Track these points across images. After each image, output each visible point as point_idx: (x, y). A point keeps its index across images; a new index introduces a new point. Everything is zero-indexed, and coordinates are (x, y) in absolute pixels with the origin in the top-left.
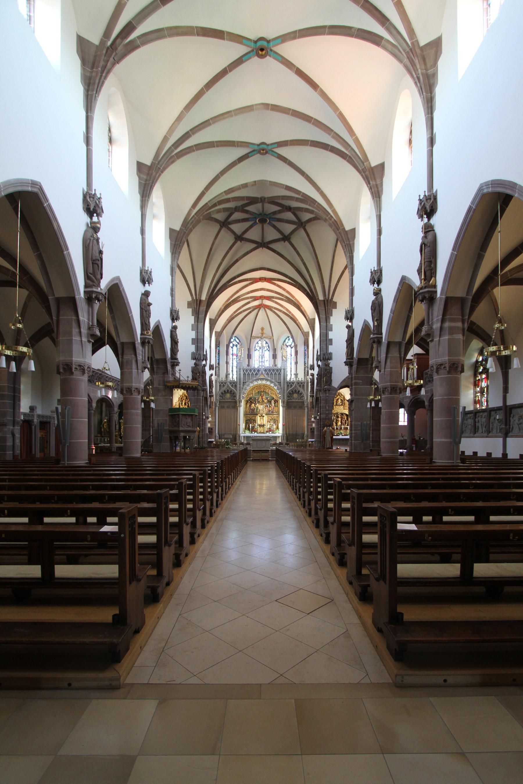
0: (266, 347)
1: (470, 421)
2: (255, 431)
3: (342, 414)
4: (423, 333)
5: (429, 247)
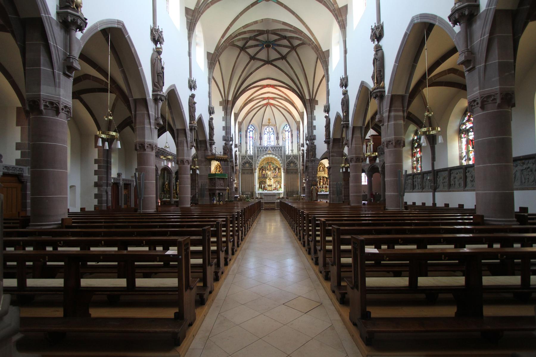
0: (272, 132)
1: (410, 181)
2: (266, 190)
3: (323, 177)
4: (377, 120)
5: (379, 61)
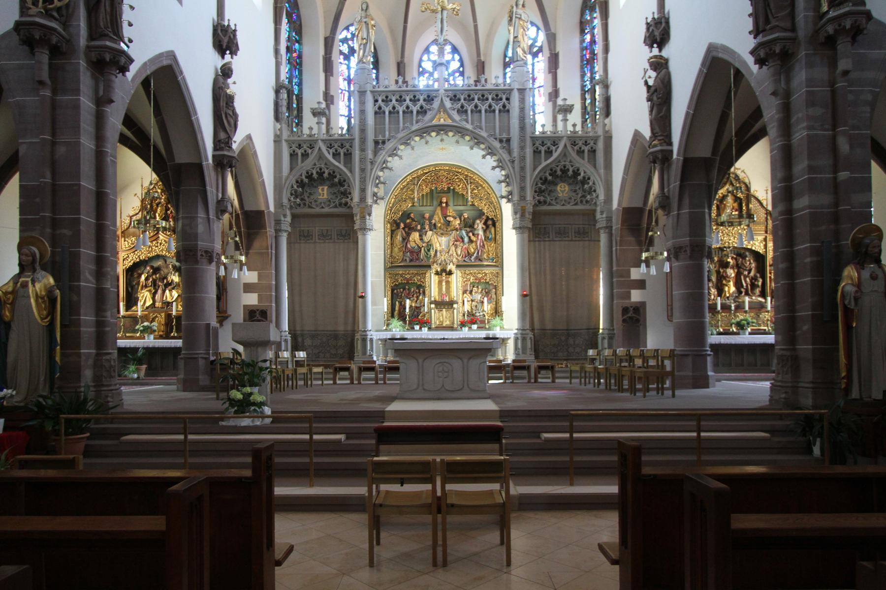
2: (425, 323)
3: (741, 253)
